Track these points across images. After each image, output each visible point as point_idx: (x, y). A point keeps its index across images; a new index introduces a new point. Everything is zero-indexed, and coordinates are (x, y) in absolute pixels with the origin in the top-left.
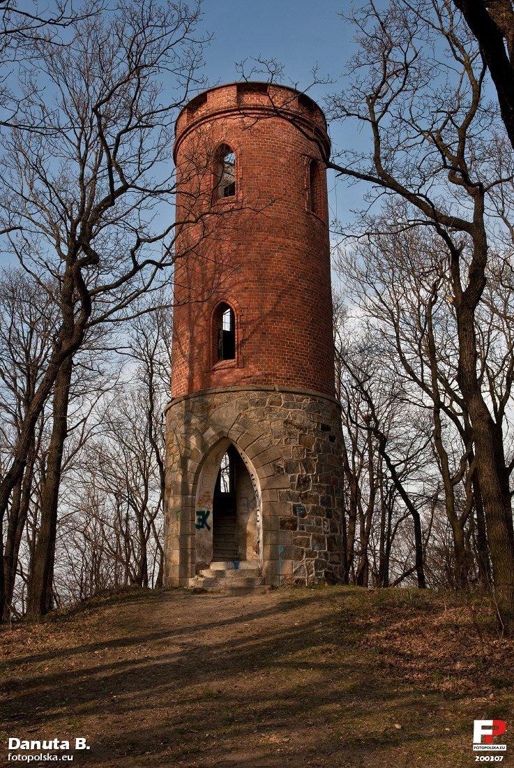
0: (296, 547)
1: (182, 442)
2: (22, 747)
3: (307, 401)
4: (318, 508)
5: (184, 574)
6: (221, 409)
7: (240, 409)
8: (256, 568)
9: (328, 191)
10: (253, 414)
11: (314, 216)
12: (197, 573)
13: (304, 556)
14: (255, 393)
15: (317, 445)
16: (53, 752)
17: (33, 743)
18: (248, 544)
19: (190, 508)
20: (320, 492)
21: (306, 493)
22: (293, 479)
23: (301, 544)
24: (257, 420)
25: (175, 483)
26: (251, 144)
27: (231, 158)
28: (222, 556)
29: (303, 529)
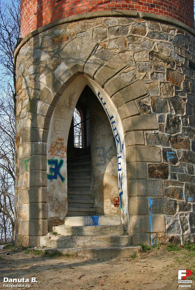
0: (169, 199)
1: (31, 84)
2: (9, 281)
3: (174, 33)
4: (189, 154)
5: (35, 232)
6: (75, 40)
8: (118, 223)
10: (112, 44)
12: (50, 230)
13: (178, 209)
14: (116, 19)
15: (186, 83)
17: (14, 280)
18: (105, 197)
19: (41, 156)
20: (191, 136)
21: (176, 136)
22: (161, 119)
23: (173, 195)
24: (118, 51)
25: (24, 129)
28: (77, 209)
29: (175, 178)
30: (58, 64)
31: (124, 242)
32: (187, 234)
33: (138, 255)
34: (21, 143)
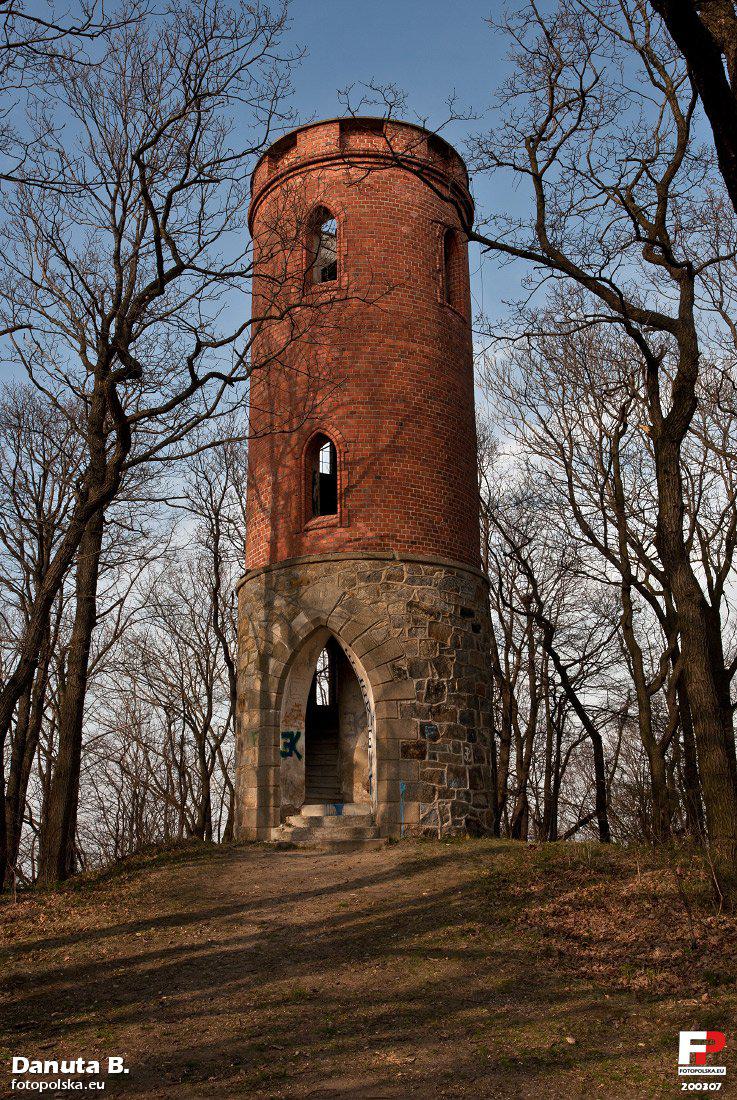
0: (425, 783)
1: (262, 634)
2: (32, 1070)
5: (264, 822)
6: (317, 586)
7: (344, 585)
9: (471, 273)
10: (363, 593)
11: (451, 309)
12: (283, 821)
14: (366, 563)
15: (455, 638)
16: (75, 1077)
17: (48, 1064)
18: (355, 779)
19: (273, 728)
20: (459, 705)
21: (439, 706)
22: (420, 686)
23: (431, 779)
24: (368, 602)
26: (360, 207)
27: (331, 226)
28: (318, 796)
29: (435, 758)
30: (296, 614)
31: (370, 835)
32: (447, 826)
33: (384, 848)
34: (246, 708)
